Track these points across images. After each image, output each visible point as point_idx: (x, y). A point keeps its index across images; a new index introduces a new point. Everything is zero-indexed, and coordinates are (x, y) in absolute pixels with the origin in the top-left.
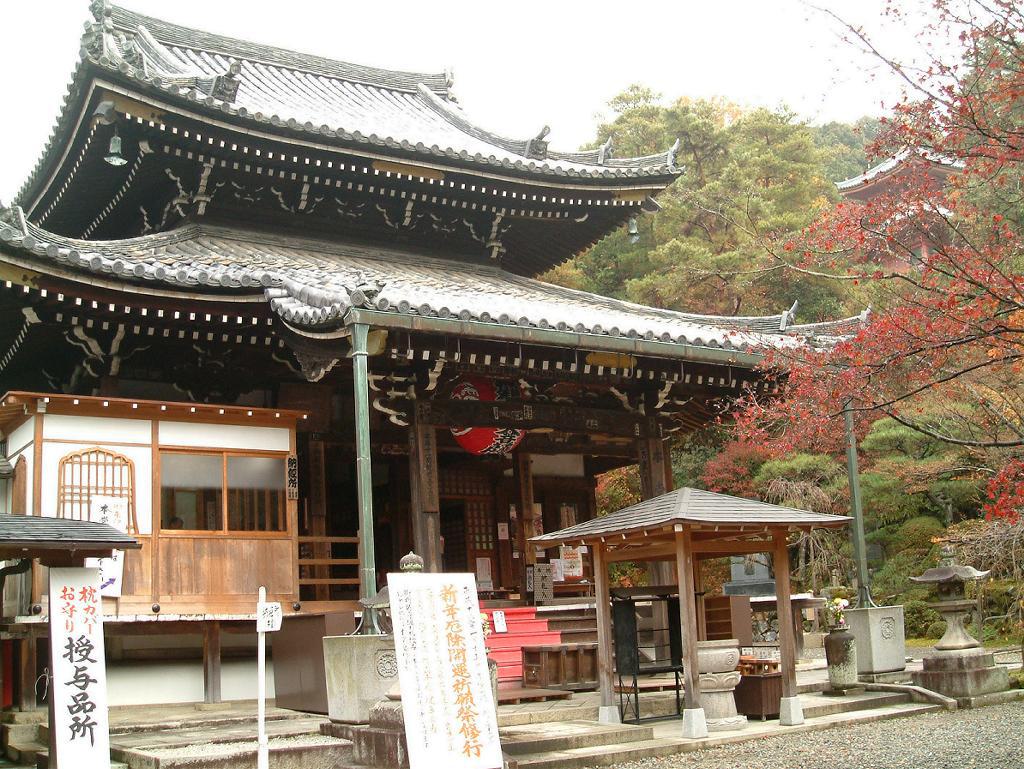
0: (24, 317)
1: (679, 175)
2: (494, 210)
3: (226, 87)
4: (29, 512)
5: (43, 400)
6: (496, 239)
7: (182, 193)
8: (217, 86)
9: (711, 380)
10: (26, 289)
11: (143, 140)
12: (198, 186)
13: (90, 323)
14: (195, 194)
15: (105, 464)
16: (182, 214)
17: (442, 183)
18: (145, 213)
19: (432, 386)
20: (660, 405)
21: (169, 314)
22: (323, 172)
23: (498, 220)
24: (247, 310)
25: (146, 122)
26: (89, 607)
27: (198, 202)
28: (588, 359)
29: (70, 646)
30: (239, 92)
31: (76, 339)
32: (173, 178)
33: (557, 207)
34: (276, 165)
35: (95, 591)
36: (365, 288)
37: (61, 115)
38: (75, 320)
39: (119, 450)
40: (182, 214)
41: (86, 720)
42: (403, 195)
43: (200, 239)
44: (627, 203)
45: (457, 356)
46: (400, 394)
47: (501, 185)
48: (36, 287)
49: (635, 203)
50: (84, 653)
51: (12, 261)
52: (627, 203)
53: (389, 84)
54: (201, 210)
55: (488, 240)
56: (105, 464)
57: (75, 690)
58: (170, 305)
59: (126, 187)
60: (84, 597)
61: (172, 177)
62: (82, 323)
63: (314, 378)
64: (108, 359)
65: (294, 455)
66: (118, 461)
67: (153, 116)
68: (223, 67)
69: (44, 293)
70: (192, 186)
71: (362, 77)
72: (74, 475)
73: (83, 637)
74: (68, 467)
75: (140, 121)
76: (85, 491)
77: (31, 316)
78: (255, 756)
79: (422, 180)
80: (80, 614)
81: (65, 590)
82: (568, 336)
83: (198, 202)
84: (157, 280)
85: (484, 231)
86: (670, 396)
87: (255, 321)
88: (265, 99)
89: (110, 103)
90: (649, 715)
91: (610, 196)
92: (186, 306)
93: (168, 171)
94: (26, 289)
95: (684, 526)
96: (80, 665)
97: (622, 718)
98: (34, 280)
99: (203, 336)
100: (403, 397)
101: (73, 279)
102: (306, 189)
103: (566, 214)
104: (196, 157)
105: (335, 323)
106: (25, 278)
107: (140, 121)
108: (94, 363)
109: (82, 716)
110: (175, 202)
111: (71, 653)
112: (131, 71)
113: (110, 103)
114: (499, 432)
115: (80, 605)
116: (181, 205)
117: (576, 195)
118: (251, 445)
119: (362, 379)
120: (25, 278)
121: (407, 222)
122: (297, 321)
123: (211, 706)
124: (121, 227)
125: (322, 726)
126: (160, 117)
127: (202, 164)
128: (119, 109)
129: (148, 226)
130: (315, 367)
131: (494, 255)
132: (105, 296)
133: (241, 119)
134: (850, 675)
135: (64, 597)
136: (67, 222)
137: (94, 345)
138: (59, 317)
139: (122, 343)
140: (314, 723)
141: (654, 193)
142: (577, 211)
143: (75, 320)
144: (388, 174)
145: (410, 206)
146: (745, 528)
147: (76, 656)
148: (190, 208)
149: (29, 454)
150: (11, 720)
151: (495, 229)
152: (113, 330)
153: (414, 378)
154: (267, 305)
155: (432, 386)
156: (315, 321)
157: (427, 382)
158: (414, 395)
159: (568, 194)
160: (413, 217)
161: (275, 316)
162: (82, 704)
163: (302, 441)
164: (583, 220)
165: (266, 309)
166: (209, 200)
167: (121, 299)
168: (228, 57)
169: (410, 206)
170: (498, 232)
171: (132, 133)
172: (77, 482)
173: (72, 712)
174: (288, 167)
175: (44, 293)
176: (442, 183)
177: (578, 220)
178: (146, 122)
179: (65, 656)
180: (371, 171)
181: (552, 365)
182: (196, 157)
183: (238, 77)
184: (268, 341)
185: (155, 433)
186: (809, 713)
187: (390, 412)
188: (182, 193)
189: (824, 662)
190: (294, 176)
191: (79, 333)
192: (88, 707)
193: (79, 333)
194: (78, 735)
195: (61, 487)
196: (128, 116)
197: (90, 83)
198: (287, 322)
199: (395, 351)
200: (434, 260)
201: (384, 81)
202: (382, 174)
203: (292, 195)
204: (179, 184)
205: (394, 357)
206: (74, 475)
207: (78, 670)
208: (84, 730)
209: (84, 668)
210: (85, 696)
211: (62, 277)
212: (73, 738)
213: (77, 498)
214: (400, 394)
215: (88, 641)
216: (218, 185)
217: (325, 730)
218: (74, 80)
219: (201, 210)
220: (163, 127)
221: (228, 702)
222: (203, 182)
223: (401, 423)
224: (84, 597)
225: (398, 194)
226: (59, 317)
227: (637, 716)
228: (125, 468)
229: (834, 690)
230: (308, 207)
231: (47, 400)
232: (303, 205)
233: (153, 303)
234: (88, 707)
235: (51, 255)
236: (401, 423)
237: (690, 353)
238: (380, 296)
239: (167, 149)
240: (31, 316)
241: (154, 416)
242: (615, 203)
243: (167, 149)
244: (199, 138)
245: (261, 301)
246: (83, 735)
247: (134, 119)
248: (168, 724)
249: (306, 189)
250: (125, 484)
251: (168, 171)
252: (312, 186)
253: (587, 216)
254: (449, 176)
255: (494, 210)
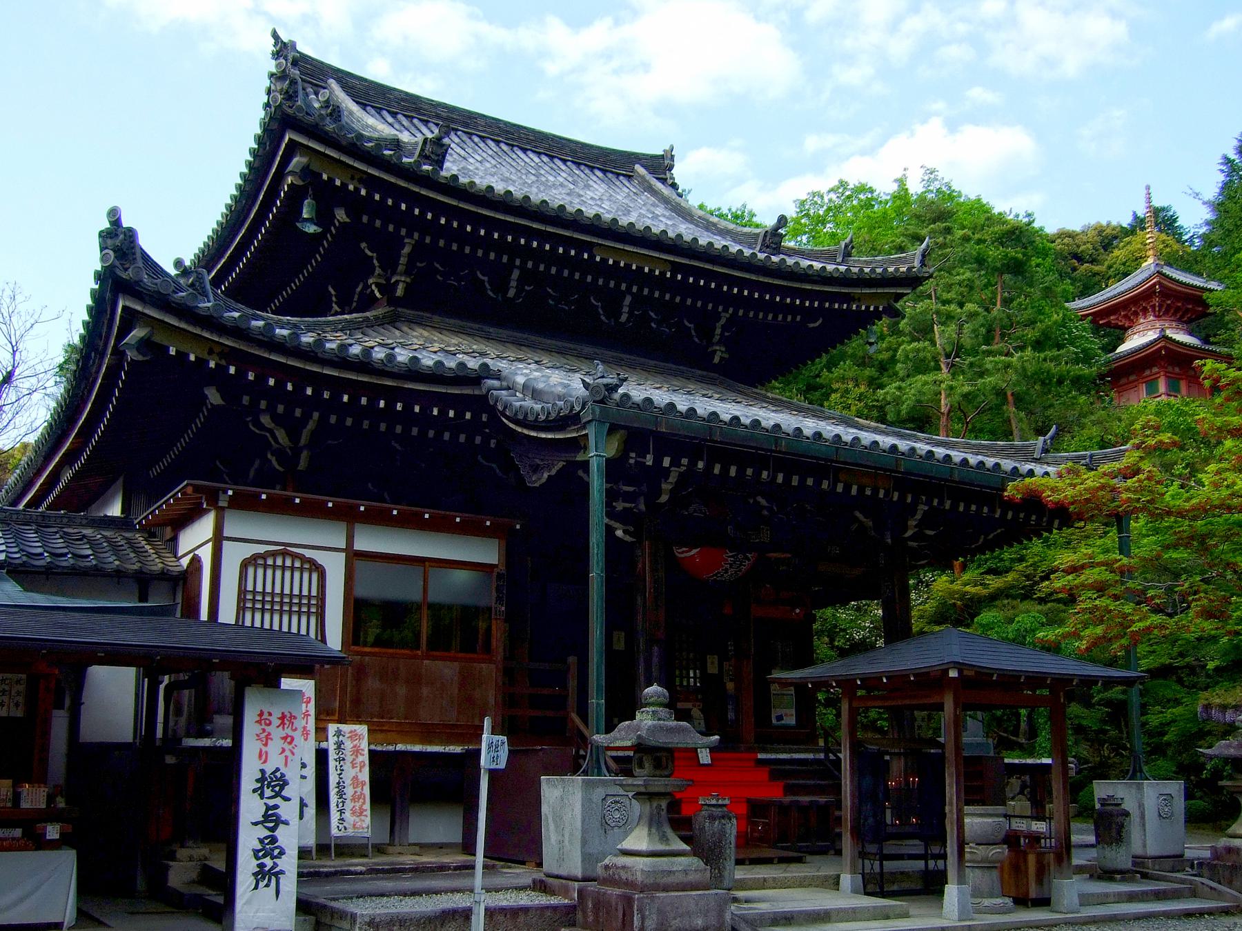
0: (206, 397)
1: (928, 278)
2: (720, 309)
3: (436, 152)
4: (204, 615)
5: (225, 492)
6: (719, 343)
7: (378, 271)
8: (422, 150)
9: (973, 507)
10: (212, 364)
11: (339, 206)
12: (398, 264)
13: (281, 409)
14: (394, 273)
15: (293, 569)
16: (378, 295)
17: (668, 275)
18: (333, 292)
19: (664, 498)
20: (909, 533)
21: (373, 402)
22: (538, 255)
23: (723, 321)
24: (461, 403)
25: (344, 185)
26: (288, 736)
27: (397, 282)
28: (842, 476)
29: (261, 780)
30: (448, 157)
31: (261, 427)
32: (369, 254)
33: (792, 309)
34: (487, 243)
35: (295, 718)
36: (605, 381)
37: (246, 170)
38: (263, 404)
39: (308, 553)
40: (378, 295)
41: (272, 868)
42: (623, 287)
43: (398, 324)
44: (868, 307)
45: (701, 465)
46: (628, 505)
47: (733, 281)
48: (223, 362)
49: (876, 308)
50: (277, 789)
51: (197, 331)
52: (868, 307)
53: (604, 163)
54: (400, 292)
55: (711, 344)
56: (293, 569)
57: (263, 832)
58: (375, 392)
59: (316, 261)
60: (283, 723)
61: (369, 254)
62: (271, 410)
63: (535, 482)
64: (297, 451)
65: (502, 569)
66: (307, 566)
67: (352, 178)
68: (431, 133)
69: (232, 370)
70: (390, 265)
71: (574, 153)
72: (258, 580)
73: (278, 769)
74: (251, 571)
75: (338, 183)
76: (305, 601)
77: (213, 396)
78: (466, 914)
79: (646, 270)
80: (275, 746)
81: (261, 714)
82: (824, 449)
83: (397, 282)
84: (361, 362)
85: (707, 333)
86: (921, 525)
87: (468, 416)
88: (473, 165)
89: (304, 160)
90: (895, 888)
91: (849, 298)
92: (392, 395)
93: (363, 245)
94: (212, 364)
95: (960, 672)
96: (271, 802)
97: (865, 887)
98: (221, 355)
99: (407, 430)
100: (631, 509)
101: (266, 355)
102: (516, 274)
103: (798, 318)
104: (397, 230)
105: (569, 419)
106: (211, 352)
107: (338, 183)
108: (280, 453)
109: (268, 862)
110: (370, 281)
111: (262, 788)
112: (330, 127)
113: (304, 160)
114: (729, 555)
115: (277, 732)
116: (377, 285)
117: (811, 295)
118: (461, 556)
119: (597, 484)
120: (211, 352)
121: (624, 318)
122: (521, 417)
123: (398, 849)
124: (309, 304)
125: (534, 881)
126: (361, 181)
127: (403, 238)
128: (315, 167)
129: (335, 307)
130: (536, 469)
131: (716, 360)
132: (303, 378)
133: (452, 187)
134: (1120, 858)
135: (259, 722)
136: (251, 291)
137: (281, 435)
138: (246, 400)
139: (313, 433)
140: (524, 874)
141: (899, 297)
142: (811, 314)
143: (263, 404)
144: (611, 262)
145: (628, 299)
146: (1053, 679)
147: (268, 792)
148: (388, 289)
149: (206, 554)
150: (172, 857)
151: (718, 331)
152: (307, 417)
153: (644, 488)
154: (485, 398)
155: (664, 498)
156: (542, 417)
157: (659, 493)
158: (642, 507)
159: (805, 295)
160: (631, 313)
161: (492, 410)
162: (269, 847)
163: (510, 554)
164: (817, 324)
165: (483, 404)
166: (408, 280)
167: (320, 381)
168: (428, 122)
169: (628, 299)
170: (722, 334)
171: (327, 197)
172: (259, 588)
173: (257, 858)
174: (501, 247)
175: (232, 370)
176: (668, 275)
177: (811, 325)
178: (344, 185)
179: (254, 791)
180: (592, 257)
181: (802, 481)
182: (397, 230)
183: (446, 141)
184: (478, 440)
185: (350, 540)
186: (1085, 900)
187: (616, 525)
188: (378, 271)
189: (1092, 839)
190: (505, 259)
191: (266, 420)
192: (276, 852)
193: (266, 420)
194: (261, 884)
195: (242, 592)
196: (325, 177)
197: (282, 137)
198: (507, 418)
199: (633, 455)
200: (652, 362)
201: (597, 161)
202: (604, 261)
203: (500, 277)
204: (375, 262)
205: (632, 461)
206: (258, 580)
207: (268, 808)
208: (270, 880)
209: (276, 807)
210: (274, 840)
211: (254, 353)
212: (256, 887)
213: (295, 609)
214: (628, 505)
215: (283, 775)
216: (419, 264)
217: (540, 887)
218: (259, 144)
219: (400, 292)
220: (363, 192)
221: (415, 844)
222: (403, 260)
223: (628, 538)
224: (283, 723)
225: (618, 285)
226: (246, 400)
227: (882, 887)
228: (315, 576)
229: (1107, 874)
230: (517, 295)
231: (230, 493)
232: (511, 293)
233: (356, 389)
234: (276, 852)
235: (244, 326)
236: (628, 538)
237: (956, 477)
238: (621, 391)
239: (365, 219)
240: (213, 396)
241: (348, 517)
242: (854, 307)
243: (365, 219)
244: (403, 207)
245: (477, 392)
246: (267, 886)
247: (331, 180)
248: (352, 869)
249: (516, 274)
250: (314, 593)
251: (363, 245)
252: (522, 268)
253: (281, 469)
254: (676, 268)
255: (720, 309)
